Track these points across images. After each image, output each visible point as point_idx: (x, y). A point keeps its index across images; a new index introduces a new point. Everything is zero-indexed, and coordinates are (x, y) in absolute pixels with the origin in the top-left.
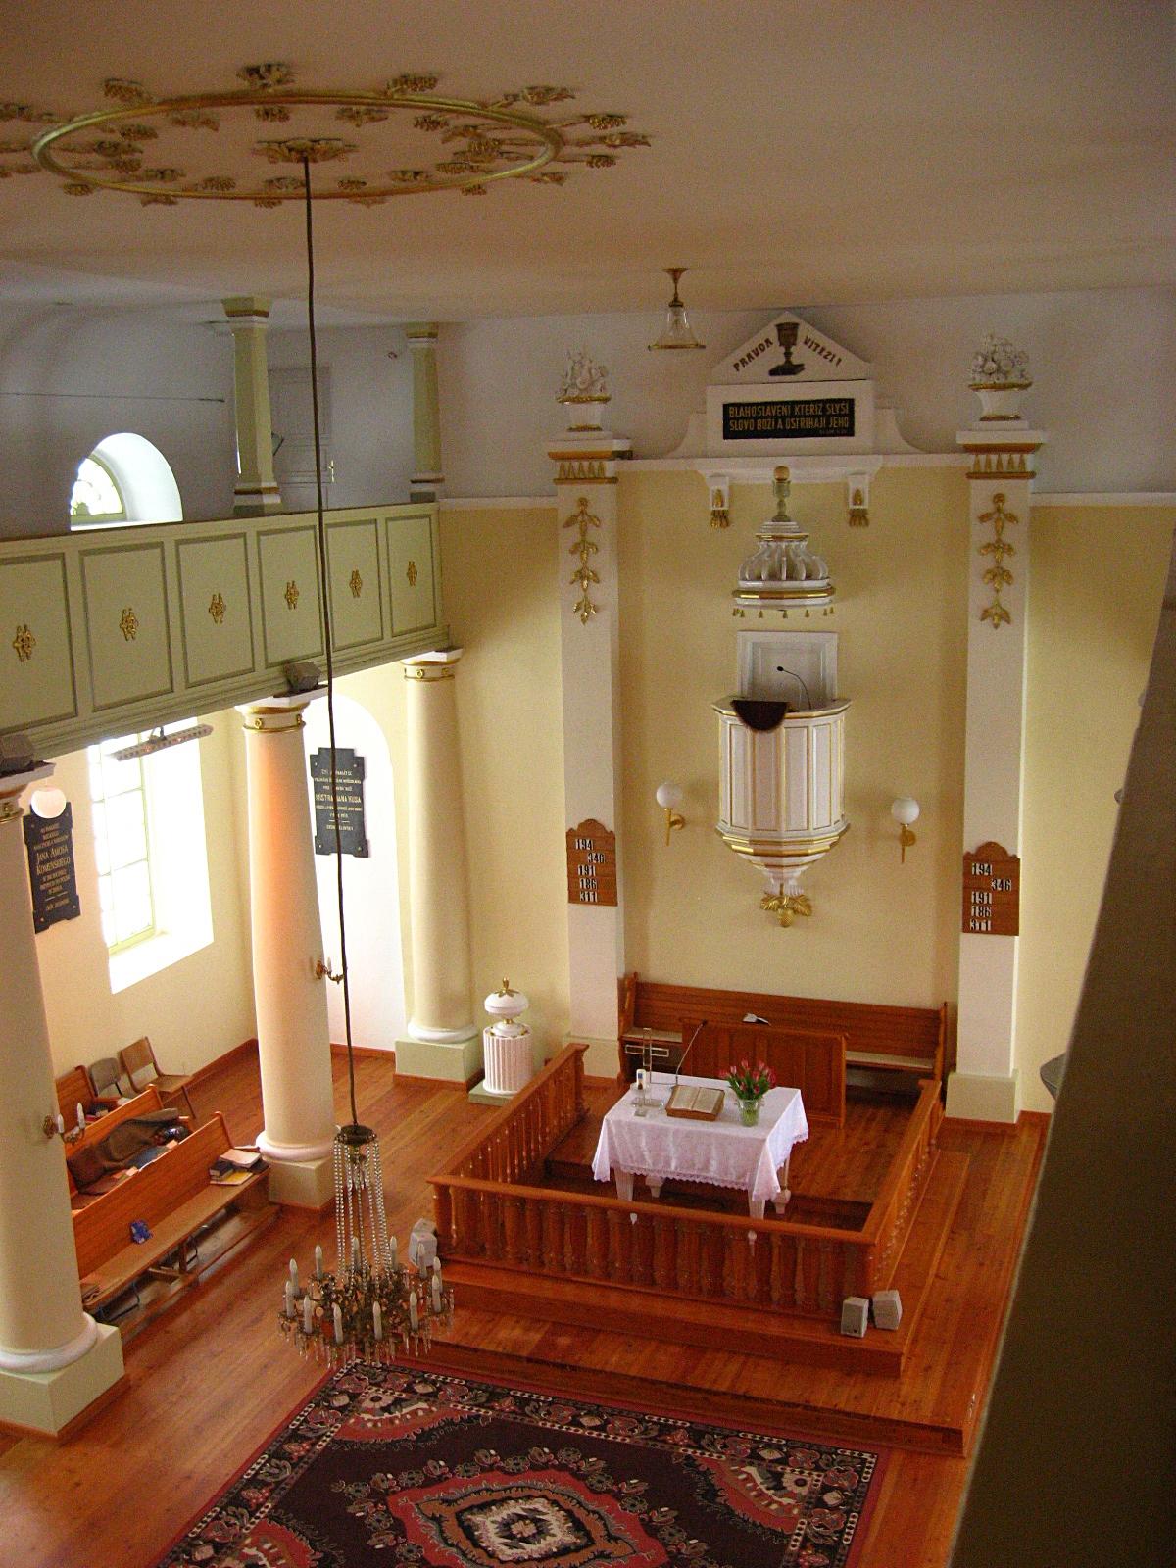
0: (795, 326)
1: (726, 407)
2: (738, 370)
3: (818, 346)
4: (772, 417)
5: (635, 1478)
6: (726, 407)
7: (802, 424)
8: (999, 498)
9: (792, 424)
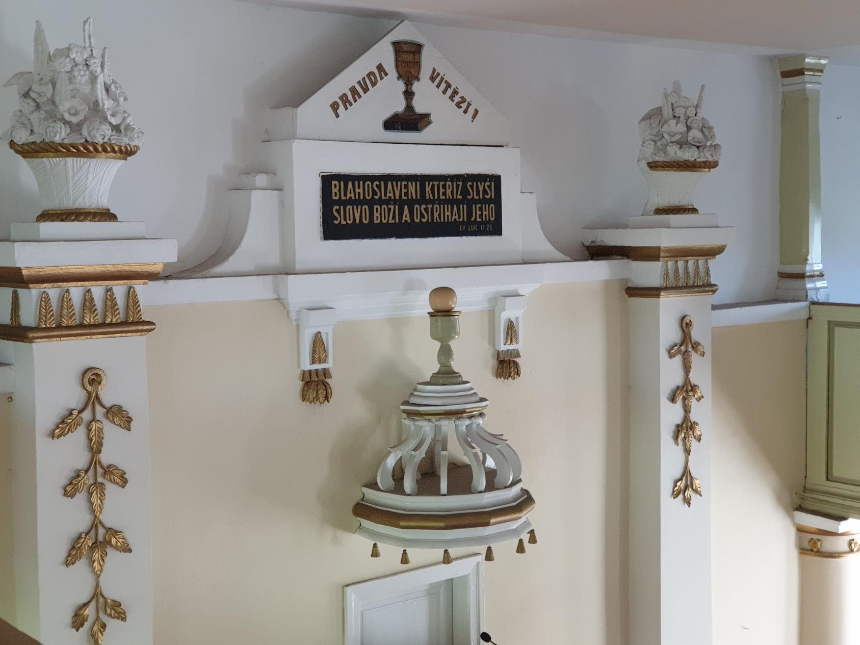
1: (327, 180)
2: (337, 116)
4: (395, 202)
6: (327, 180)
8: (92, 378)
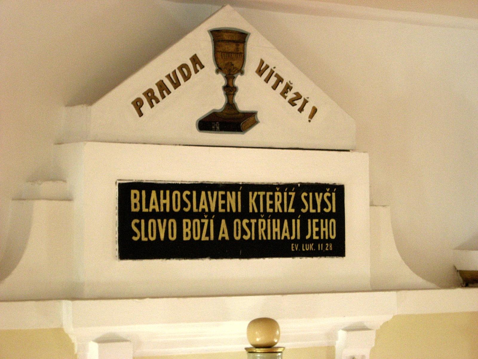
0: (241, 37)
1: (125, 189)
2: (141, 114)
3: (280, 80)
4: (210, 215)
5: (286, 188)
6: (125, 189)
7: (261, 231)
9: (243, 230)
